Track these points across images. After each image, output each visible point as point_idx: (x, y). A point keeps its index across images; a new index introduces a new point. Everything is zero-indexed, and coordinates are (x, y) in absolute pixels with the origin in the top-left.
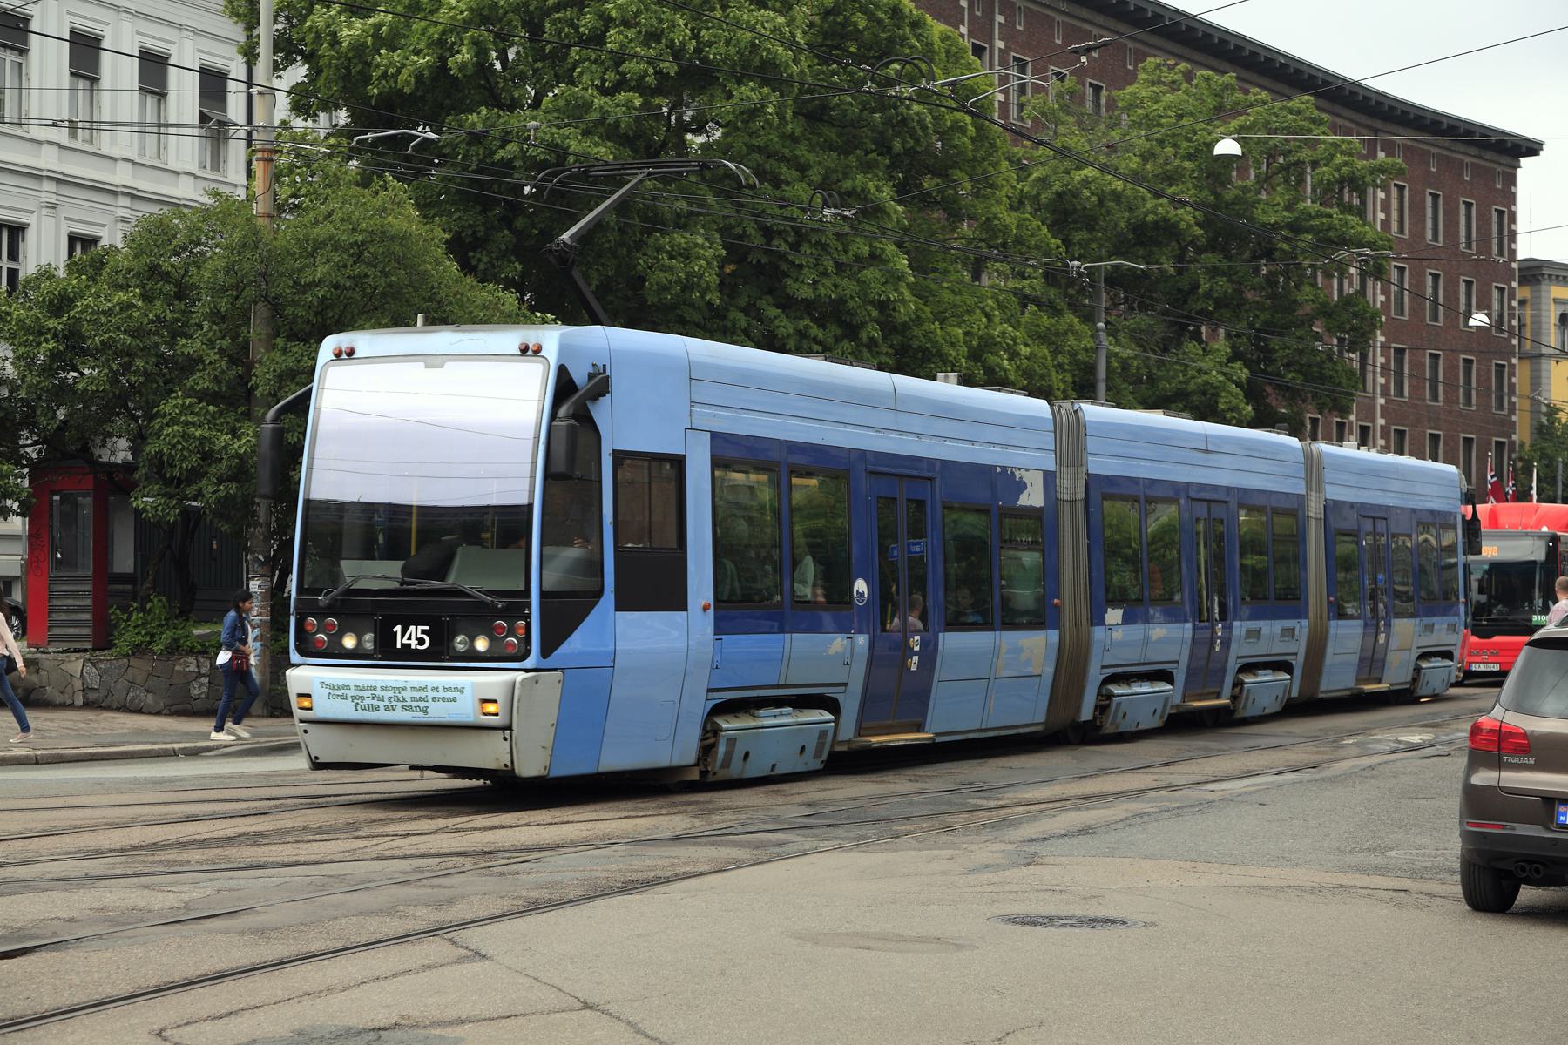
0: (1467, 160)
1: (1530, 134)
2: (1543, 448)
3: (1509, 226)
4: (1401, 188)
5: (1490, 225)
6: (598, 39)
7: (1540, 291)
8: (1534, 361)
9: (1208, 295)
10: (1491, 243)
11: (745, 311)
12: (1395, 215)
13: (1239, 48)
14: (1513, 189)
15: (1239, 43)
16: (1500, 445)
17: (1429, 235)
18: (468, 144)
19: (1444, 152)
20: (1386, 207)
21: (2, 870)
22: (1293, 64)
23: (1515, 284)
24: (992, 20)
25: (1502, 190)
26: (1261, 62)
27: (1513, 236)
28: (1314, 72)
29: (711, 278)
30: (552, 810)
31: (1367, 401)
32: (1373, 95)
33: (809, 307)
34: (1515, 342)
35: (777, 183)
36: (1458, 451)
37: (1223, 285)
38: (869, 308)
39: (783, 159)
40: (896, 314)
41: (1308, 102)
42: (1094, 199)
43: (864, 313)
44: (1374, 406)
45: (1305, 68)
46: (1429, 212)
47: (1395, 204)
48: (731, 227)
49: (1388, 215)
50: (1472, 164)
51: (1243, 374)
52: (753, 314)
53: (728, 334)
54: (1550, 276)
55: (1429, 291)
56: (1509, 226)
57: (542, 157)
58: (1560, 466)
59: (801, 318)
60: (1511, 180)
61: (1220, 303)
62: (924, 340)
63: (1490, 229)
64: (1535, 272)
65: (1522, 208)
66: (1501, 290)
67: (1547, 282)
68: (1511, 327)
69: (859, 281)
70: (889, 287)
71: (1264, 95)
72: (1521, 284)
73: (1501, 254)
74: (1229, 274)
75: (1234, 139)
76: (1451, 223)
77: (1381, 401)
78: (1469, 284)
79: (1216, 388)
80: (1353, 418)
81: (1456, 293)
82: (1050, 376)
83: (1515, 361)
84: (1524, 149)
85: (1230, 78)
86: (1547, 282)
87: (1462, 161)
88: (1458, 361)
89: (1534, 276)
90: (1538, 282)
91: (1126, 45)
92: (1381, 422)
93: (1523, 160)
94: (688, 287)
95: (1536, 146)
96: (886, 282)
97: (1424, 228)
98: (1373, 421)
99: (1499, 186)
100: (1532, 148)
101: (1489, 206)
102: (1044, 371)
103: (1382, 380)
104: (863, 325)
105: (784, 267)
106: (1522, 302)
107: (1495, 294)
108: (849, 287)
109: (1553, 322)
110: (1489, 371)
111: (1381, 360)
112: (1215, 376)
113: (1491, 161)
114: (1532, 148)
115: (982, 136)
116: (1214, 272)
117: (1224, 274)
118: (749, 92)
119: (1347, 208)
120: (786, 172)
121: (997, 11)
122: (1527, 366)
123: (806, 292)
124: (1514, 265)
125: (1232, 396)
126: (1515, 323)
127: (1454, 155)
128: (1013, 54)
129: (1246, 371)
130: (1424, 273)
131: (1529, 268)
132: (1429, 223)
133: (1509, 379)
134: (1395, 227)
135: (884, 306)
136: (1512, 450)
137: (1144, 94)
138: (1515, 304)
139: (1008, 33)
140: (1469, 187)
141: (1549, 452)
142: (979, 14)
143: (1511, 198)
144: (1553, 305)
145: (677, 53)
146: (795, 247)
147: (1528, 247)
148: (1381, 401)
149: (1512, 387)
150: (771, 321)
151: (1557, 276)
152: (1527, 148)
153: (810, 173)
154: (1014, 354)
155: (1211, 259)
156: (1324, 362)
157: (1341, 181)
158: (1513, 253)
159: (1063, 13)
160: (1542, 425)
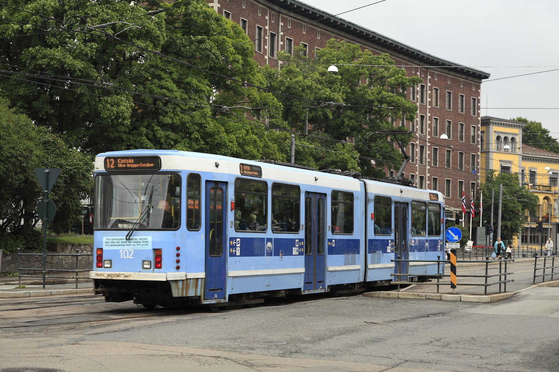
0: (462, 80)
1: (485, 70)
2: (488, 186)
3: (477, 104)
4: (437, 90)
5: (470, 104)
6: (83, 22)
7: (489, 128)
8: (487, 153)
9: (348, 126)
10: (470, 110)
11: (147, 127)
12: (434, 99)
13: (374, 37)
14: (479, 91)
15: (374, 35)
16: (473, 184)
17: (447, 106)
18: (31, 60)
19: (453, 77)
20: (431, 97)
21: (557, 294)
22: (395, 43)
23: (479, 125)
24: (279, 24)
25: (475, 91)
26: (376, 40)
27: (479, 108)
28: (403, 46)
29: (128, 114)
30: (170, 316)
31: (423, 167)
32: (426, 55)
33: (173, 128)
34: (479, 146)
35: (160, 78)
36: (457, 186)
37: (353, 123)
38: (195, 126)
39: (163, 70)
40: (207, 129)
41: (387, 55)
42: (300, 89)
43: (193, 128)
44: (426, 169)
45: (399, 45)
46: (447, 99)
47: (434, 95)
48: (139, 96)
49: (432, 99)
50: (463, 81)
51: (357, 155)
52: (150, 128)
53: (140, 136)
54: (493, 123)
55: (459, 129)
56: (477, 104)
57: (56, 66)
58: (493, 192)
59: (168, 131)
60: (478, 87)
61: (353, 129)
62: (220, 140)
63: (470, 105)
64: (487, 122)
65: (482, 97)
66: (474, 127)
67: (492, 125)
68: (478, 141)
69: (191, 116)
70: (202, 119)
71: (370, 53)
72: (482, 125)
73: (474, 114)
74: (356, 119)
75: (335, 66)
76: (456, 103)
77: (428, 167)
78: (462, 125)
79: (347, 160)
80: (417, 173)
81: (457, 128)
82: (275, 154)
83: (479, 153)
84: (483, 76)
85: (357, 45)
86: (492, 125)
87: (460, 80)
88: (457, 153)
89: (487, 122)
90: (489, 125)
91: (331, 35)
92: (428, 175)
93: (483, 80)
94: (117, 118)
95: (487, 75)
96: (202, 116)
97: (445, 104)
98: (425, 174)
99: (474, 90)
100: (486, 76)
101: (470, 97)
102: (273, 152)
103: (428, 160)
104: (193, 132)
105: (160, 111)
106: (482, 132)
107: (472, 129)
108: (187, 118)
109: (494, 139)
110: (469, 157)
111: (428, 152)
112: (347, 156)
113: (470, 80)
114: (486, 76)
115: (246, 64)
116: (351, 118)
117: (354, 119)
118: (141, 43)
119: (398, 94)
120: (163, 75)
121: (280, 21)
122: (484, 155)
123: (168, 120)
124: (479, 119)
125: (354, 163)
126: (479, 139)
127: (457, 78)
128: (286, 37)
129: (358, 154)
130: (445, 121)
131: (485, 120)
132: (447, 102)
133: (477, 160)
134: (434, 103)
135: (201, 125)
136: (478, 186)
137: (327, 51)
138: (479, 132)
139: (285, 30)
140: (462, 90)
141: (490, 187)
142: (273, 22)
143: (478, 94)
144: (494, 133)
145: (113, 27)
146: (166, 104)
147: (483, 113)
148: (428, 167)
149: (478, 163)
150: (156, 131)
151: (517, 126)
152: (484, 76)
153: (173, 75)
154: (256, 146)
155: (349, 112)
156: (391, 151)
157: (399, 84)
158: (479, 114)
159: (306, 22)
160: (488, 177)
